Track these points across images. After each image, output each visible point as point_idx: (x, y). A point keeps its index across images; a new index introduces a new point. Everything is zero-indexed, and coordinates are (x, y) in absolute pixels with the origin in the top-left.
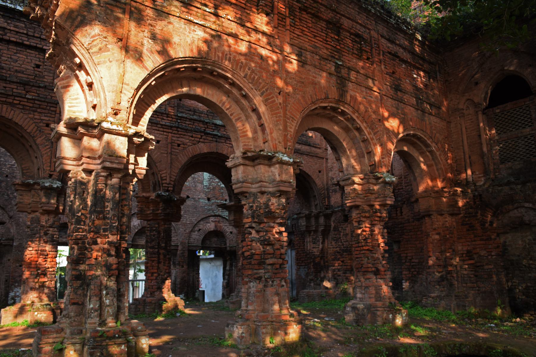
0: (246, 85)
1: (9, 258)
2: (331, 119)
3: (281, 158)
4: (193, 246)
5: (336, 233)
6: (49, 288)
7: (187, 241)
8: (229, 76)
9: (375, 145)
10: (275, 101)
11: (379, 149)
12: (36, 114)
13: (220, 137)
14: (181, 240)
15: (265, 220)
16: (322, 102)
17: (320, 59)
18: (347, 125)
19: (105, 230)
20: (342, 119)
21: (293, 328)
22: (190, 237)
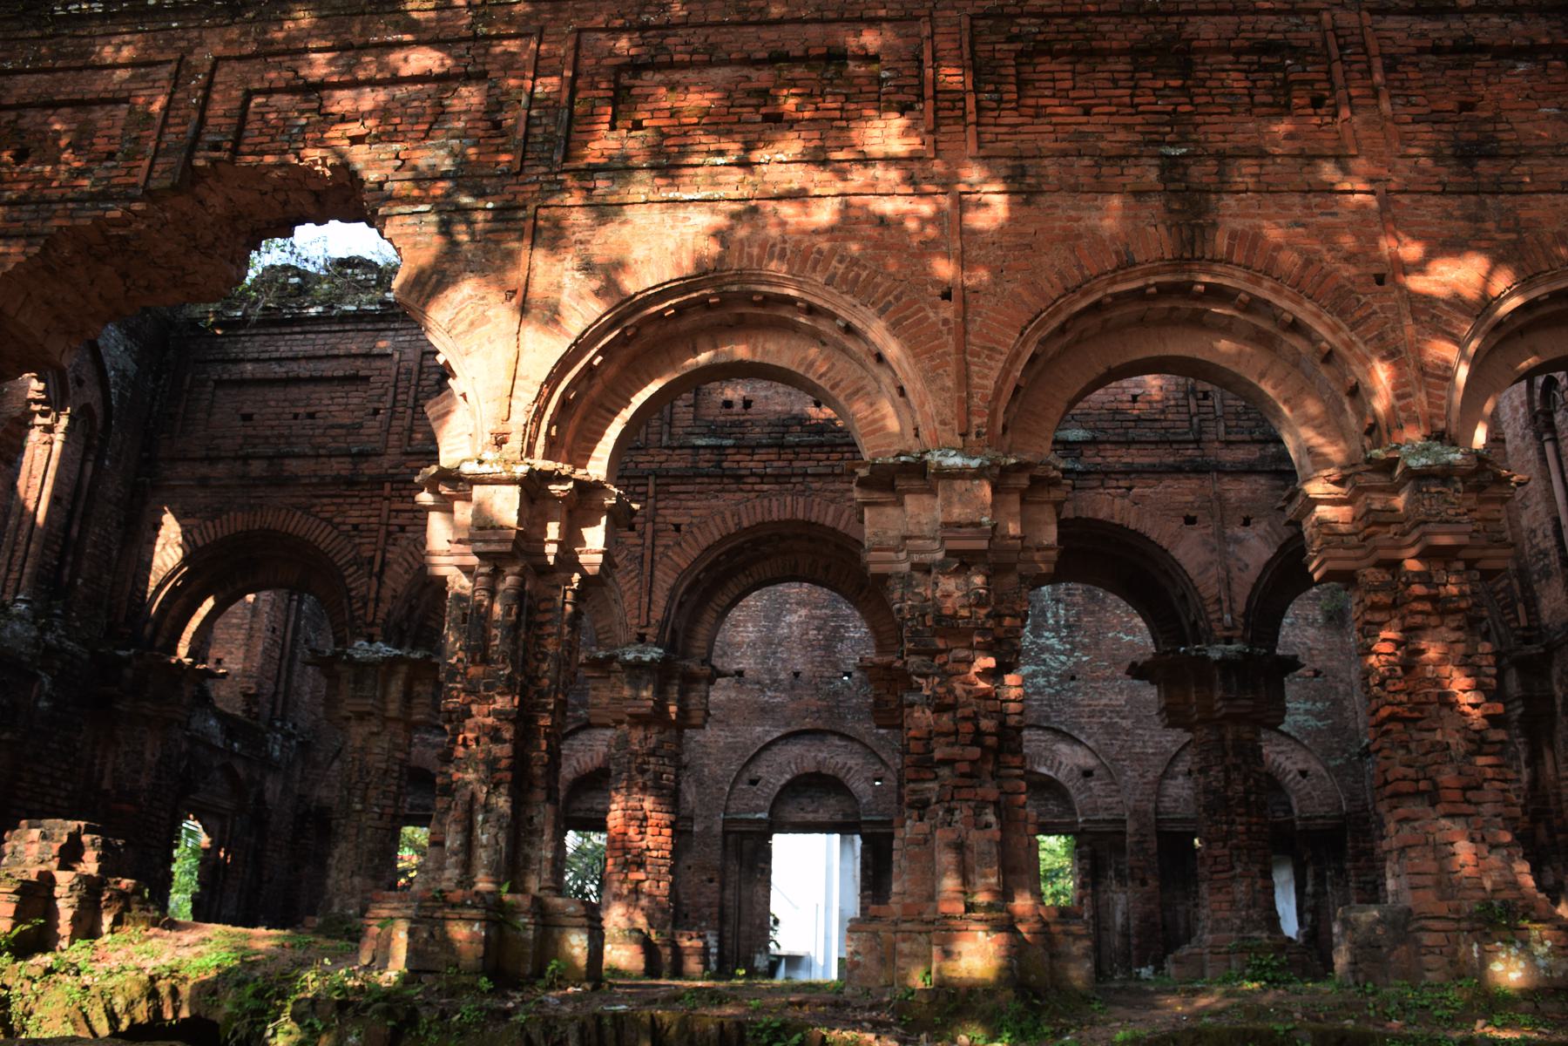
0: (839, 301)
2: (1199, 322)
3: (939, 463)
4: (1173, 820)
6: (650, 895)
7: (1151, 806)
8: (792, 292)
9: (1365, 360)
10: (927, 318)
11: (1382, 375)
13: (1082, 474)
14: (1131, 803)
15: (940, 644)
16: (1113, 282)
17: (1097, 164)
18: (1255, 326)
19: (488, 687)
20: (1228, 312)
21: (975, 939)
22: (1159, 794)
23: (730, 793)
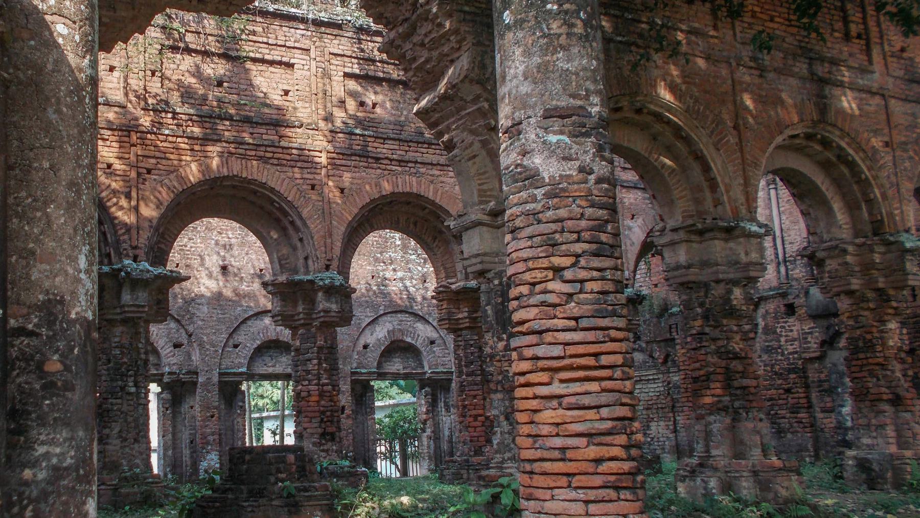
1: (192, 404)
5: (769, 338)
12: (296, 170)
23: (222, 354)
